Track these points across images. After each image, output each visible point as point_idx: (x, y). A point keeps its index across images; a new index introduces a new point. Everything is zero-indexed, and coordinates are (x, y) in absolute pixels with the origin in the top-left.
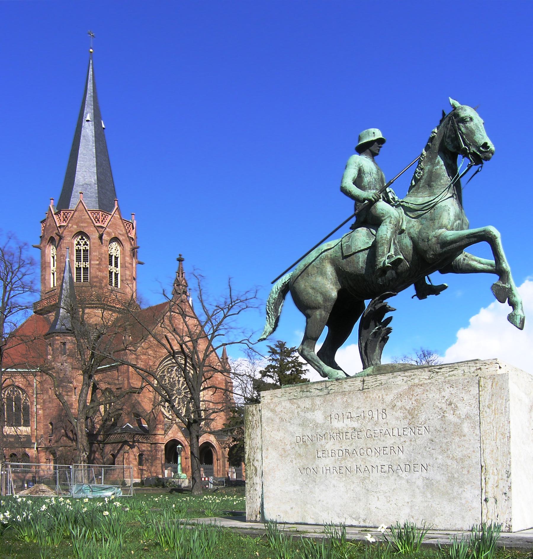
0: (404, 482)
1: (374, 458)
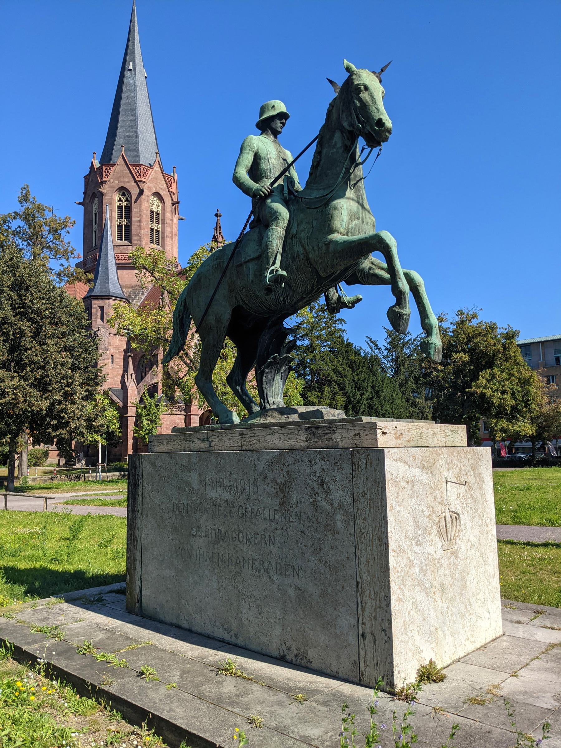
1: (245, 546)
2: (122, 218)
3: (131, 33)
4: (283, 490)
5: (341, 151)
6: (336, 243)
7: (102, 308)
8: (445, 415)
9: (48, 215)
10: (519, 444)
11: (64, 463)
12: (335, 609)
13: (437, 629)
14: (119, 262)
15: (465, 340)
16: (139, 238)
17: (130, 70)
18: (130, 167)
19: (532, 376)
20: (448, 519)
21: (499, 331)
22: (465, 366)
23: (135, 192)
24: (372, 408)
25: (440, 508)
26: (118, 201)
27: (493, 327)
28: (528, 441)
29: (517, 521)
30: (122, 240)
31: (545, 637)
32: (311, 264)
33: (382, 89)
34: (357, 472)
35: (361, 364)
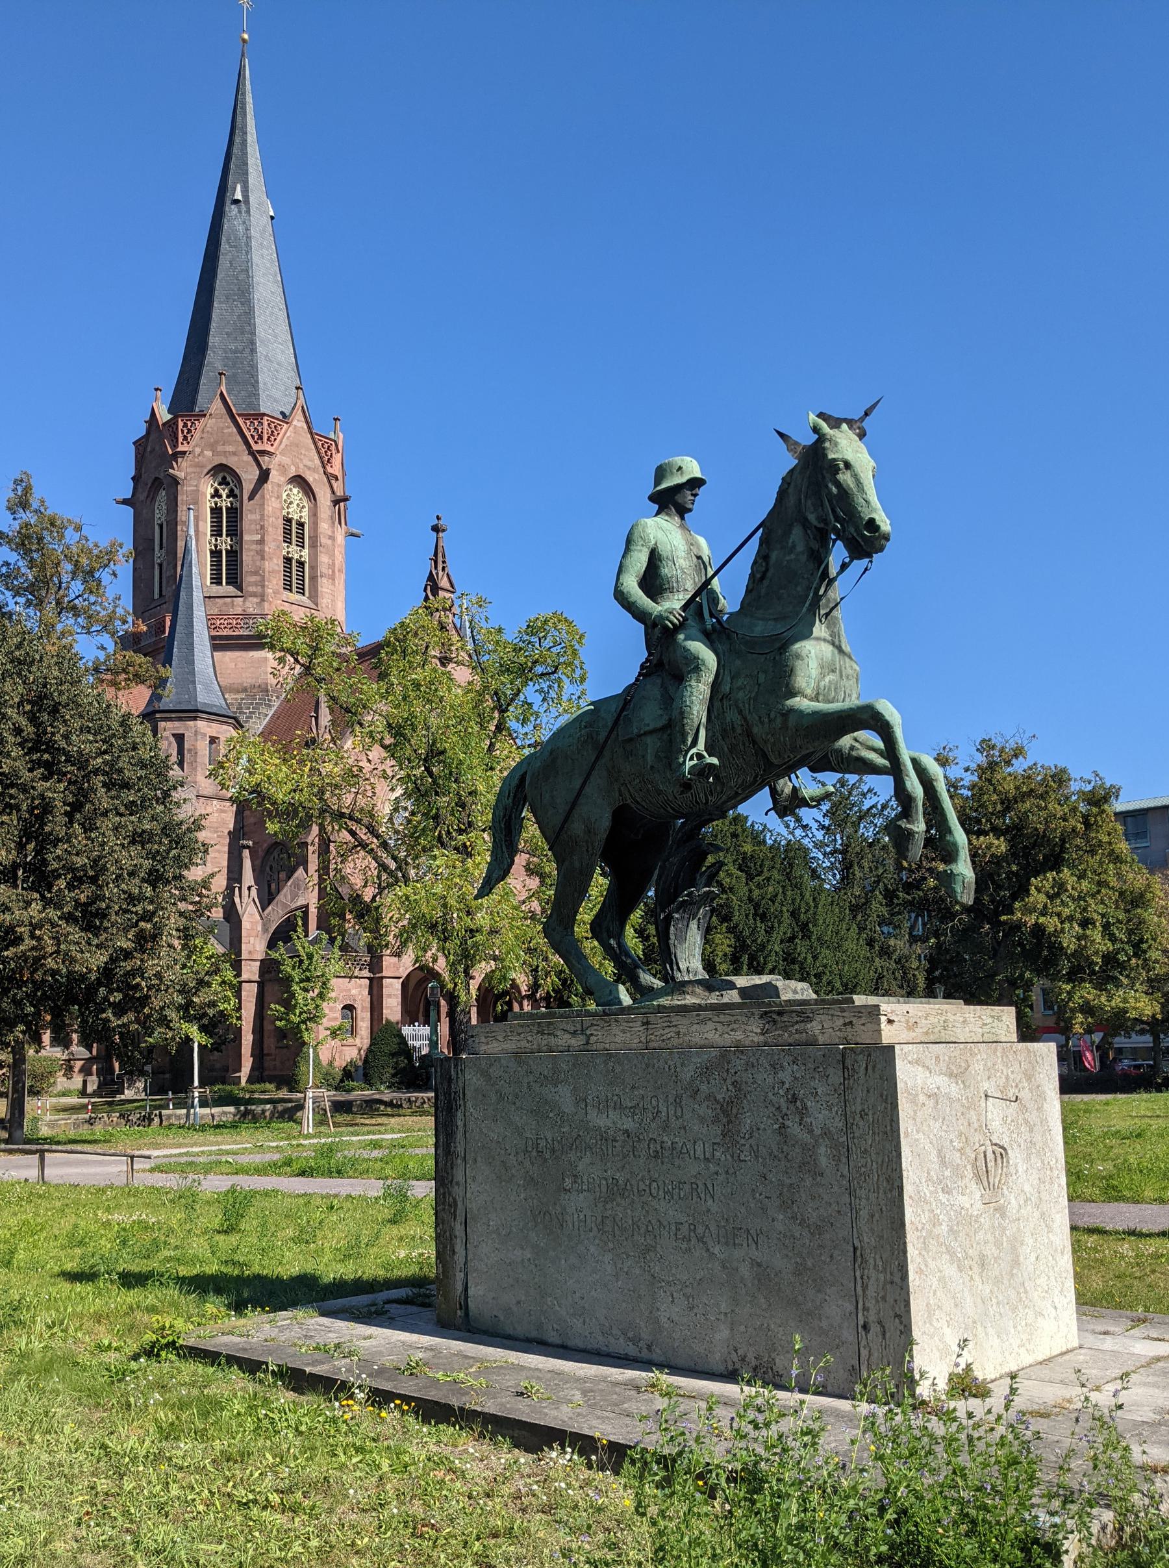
0: (717, 1266)
1: (662, 1203)
2: (221, 536)
3: (239, 118)
4: (727, 1113)
5: (804, 558)
6: (800, 713)
7: (180, 738)
8: (956, 976)
9: (71, 536)
10: (1123, 1039)
11: (95, 1087)
12: (819, 1291)
13: (975, 1322)
14: (214, 633)
15: (999, 807)
16: (258, 578)
17: (236, 202)
18: (240, 420)
19: (1149, 886)
20: (990, 1156)
21: (1074, 786)
22: (998, 864)
23: (249, 476)
24: (793, 961)
25: (977, 1138)
26: (213, 497)
27: (1060, 778)
28: (1142, 1032)
29: (1113, 1193)
30: (220, 583)
31: (1144, 1349)
32: (754, 743)
33: (872, 463)
34: (851, 1081)
35: (767, 863)
